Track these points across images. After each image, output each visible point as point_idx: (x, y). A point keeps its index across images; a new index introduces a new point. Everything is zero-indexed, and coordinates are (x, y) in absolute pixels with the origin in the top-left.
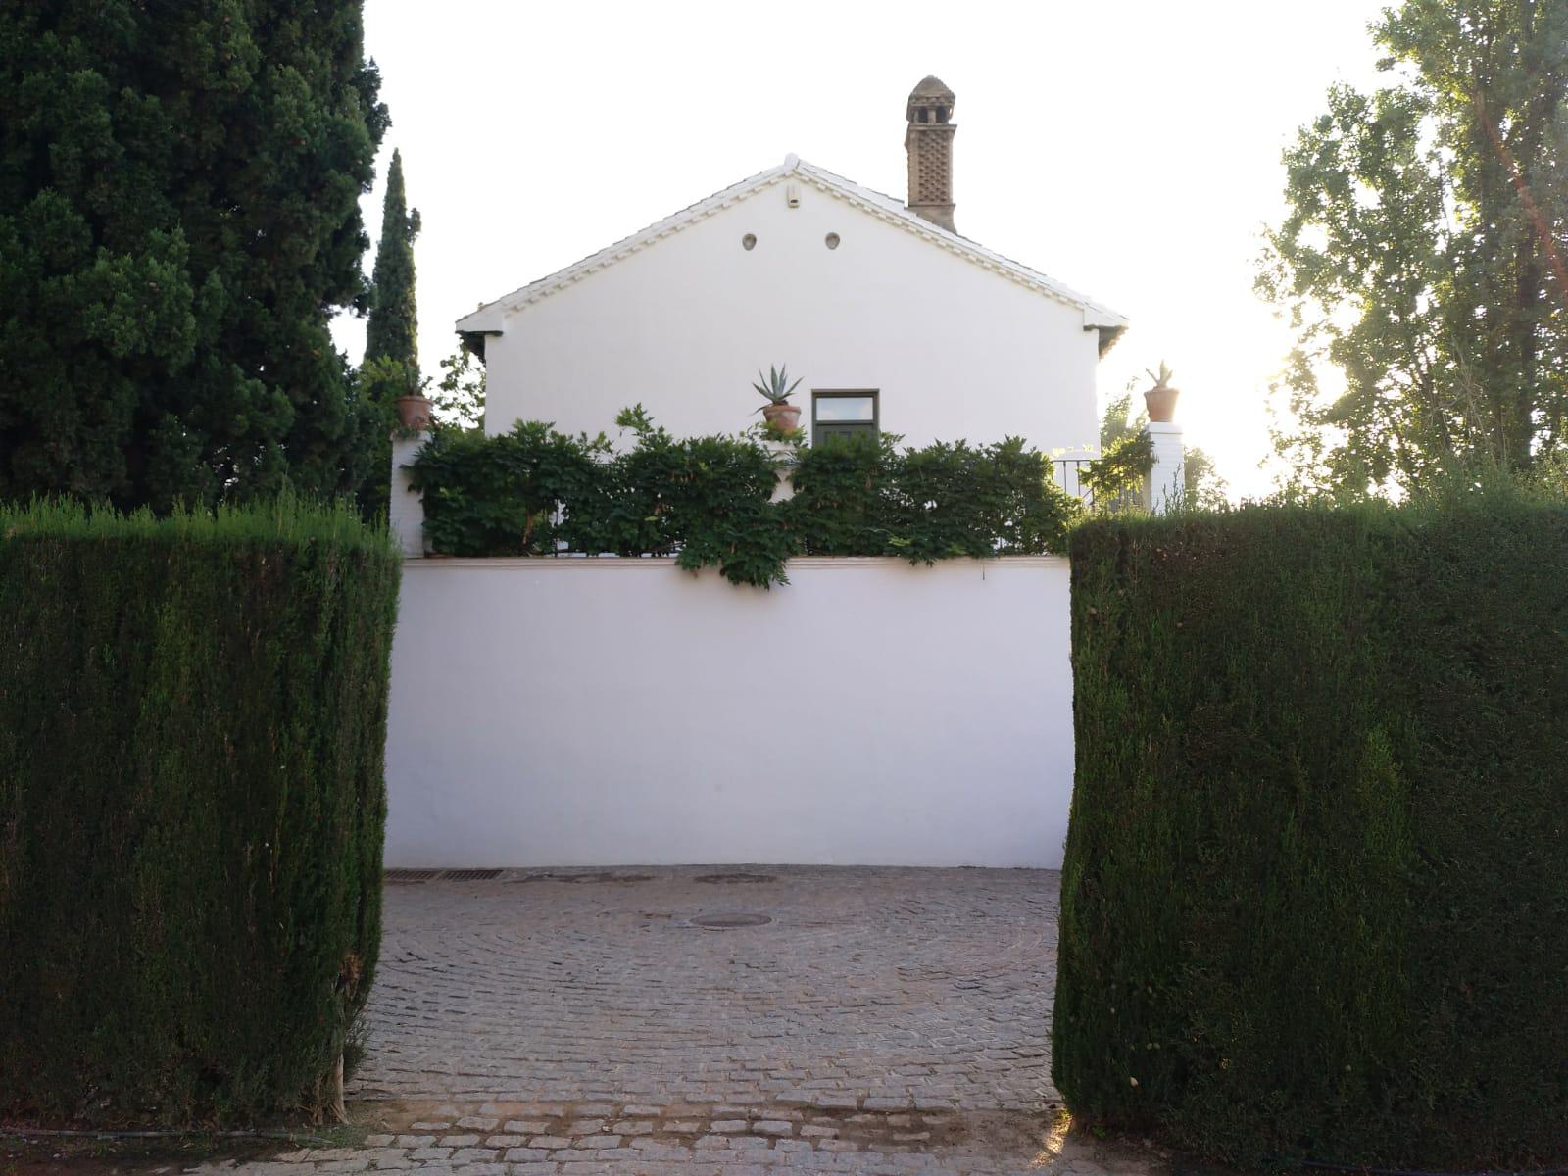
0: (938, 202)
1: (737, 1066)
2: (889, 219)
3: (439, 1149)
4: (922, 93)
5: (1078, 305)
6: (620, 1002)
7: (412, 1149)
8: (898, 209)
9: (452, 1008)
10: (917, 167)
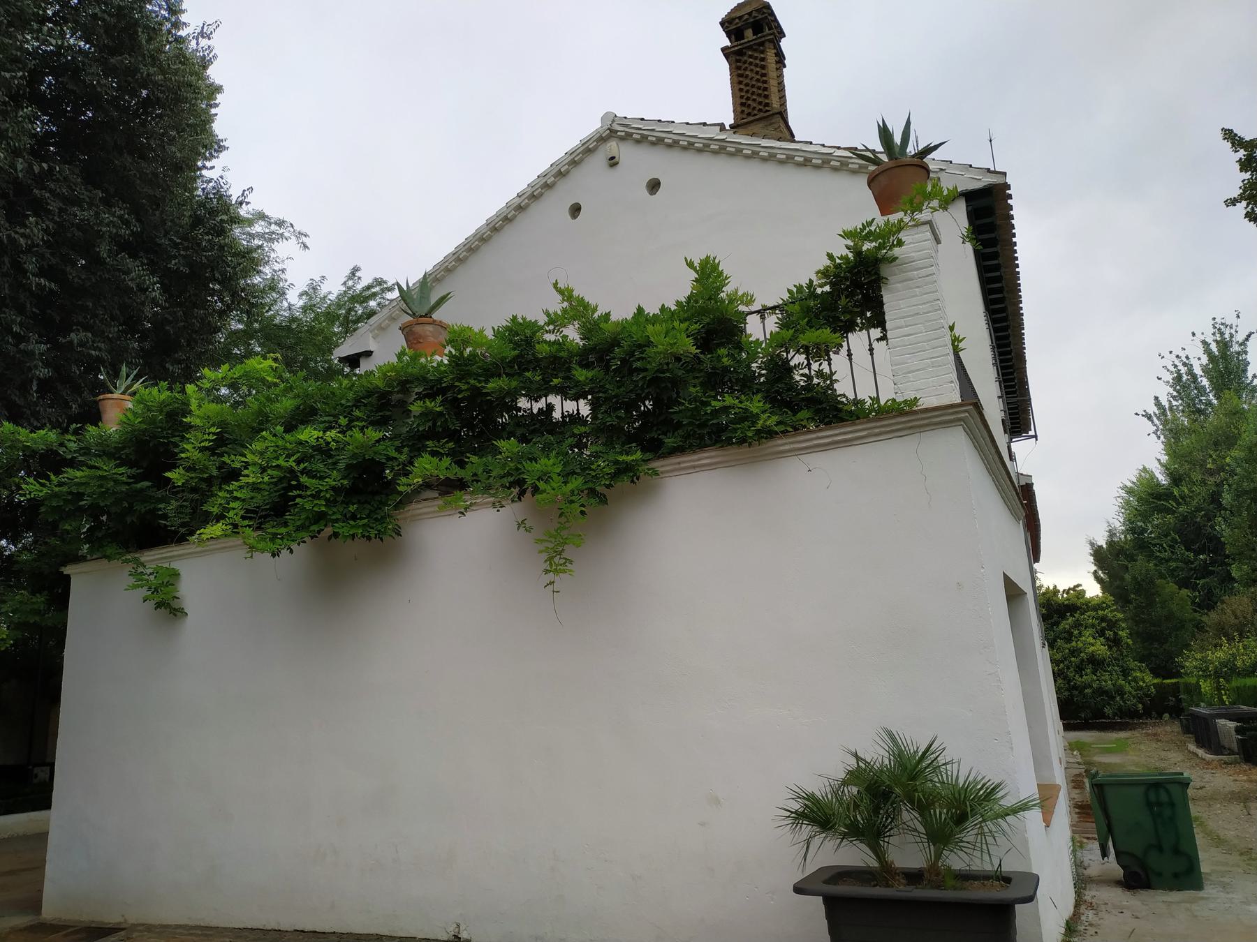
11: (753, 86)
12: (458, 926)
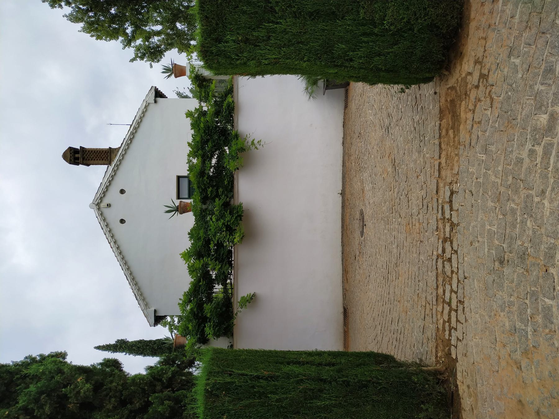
0: (109, 154)
1: (421, 212)
2: (115, 171)
3: (458, 328)
4: (69, 159)
5: (147, 105)
6: (393, 260)
7: (458, 339)
8: (111, 168)
9: (396, 324)
10: (96, 161)
11: (97, 156)
12: (339, 193)
